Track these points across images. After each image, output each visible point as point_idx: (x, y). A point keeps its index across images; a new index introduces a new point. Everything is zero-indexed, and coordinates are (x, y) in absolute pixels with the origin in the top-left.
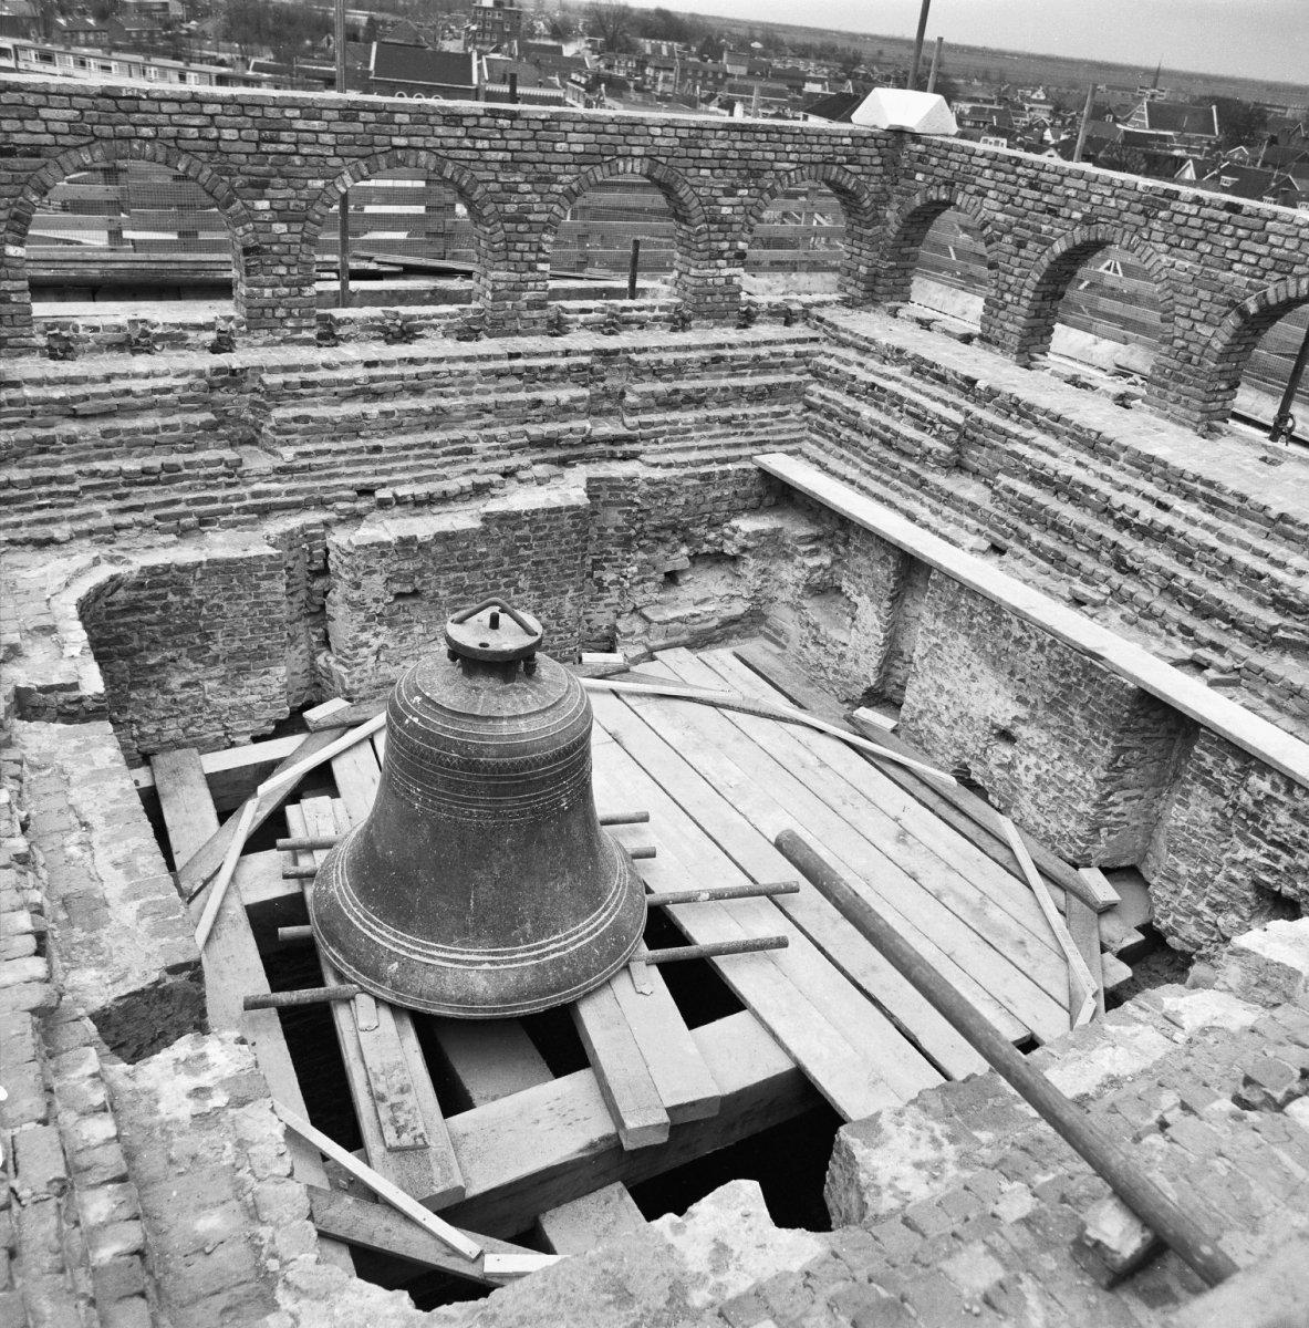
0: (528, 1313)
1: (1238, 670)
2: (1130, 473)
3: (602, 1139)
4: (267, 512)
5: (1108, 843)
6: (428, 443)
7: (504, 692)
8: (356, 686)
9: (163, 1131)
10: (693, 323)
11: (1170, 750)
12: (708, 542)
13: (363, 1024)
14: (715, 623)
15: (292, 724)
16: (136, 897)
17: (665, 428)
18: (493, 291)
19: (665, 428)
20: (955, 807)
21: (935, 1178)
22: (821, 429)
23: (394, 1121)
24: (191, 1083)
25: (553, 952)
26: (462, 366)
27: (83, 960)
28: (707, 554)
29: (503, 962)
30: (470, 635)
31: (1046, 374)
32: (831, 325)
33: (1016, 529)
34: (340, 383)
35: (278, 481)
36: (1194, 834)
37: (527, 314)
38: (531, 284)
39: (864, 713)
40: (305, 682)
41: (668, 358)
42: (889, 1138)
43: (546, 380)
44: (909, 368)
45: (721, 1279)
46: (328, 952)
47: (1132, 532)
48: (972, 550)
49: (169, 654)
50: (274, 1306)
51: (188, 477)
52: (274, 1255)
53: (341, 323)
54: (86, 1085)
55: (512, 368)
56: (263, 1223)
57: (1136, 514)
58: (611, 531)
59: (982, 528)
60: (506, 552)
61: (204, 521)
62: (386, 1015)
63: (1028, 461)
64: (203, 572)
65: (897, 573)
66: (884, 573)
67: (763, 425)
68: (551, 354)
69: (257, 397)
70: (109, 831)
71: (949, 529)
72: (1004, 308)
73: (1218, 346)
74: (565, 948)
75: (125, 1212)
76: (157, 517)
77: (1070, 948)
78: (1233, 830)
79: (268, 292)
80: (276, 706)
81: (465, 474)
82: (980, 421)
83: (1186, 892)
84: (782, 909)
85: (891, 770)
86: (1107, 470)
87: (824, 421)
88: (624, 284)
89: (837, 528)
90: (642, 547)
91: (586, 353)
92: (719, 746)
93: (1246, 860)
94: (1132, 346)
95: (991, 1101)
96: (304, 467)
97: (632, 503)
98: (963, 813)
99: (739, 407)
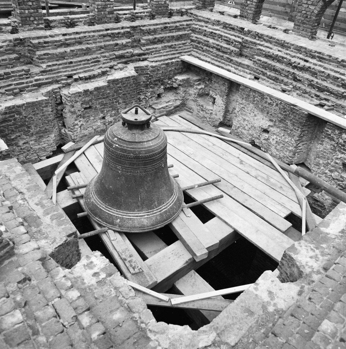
0: (226, 324)
1: (333, 106)
2: (295, 52)
3: (189, 260)
4: (40, 86)
5: (297, 157)
6: (86, 59)
7: (143, 134)
8: (75, 138)
9: (89, 289)
10: (156, 17)
11: (315, 130)
12: (168, 84)
13: (112, 239)
14: (172, 108)
15: (58, 151)
16: (48, 214)
17: (153, 50)
18: (97, 9)
19: (153, 50)
20: (252, 152)
21: (317, 260)
22: (197, 47)
23: (131, 266)
24: (92, 272)
25: (164, 209)
26: (92, 34)
27: (39, 237)
28: (168, 87)
29: (150, 214)
30: (130, 117)
31: (262, 25)
32: (195, 15)
33: (262, 72)
34: (56, 41)
35: (42, 75)
36: (325, 152)
37: (108, 16)
38: (109, 6)
39: (221, 129)
40: (58, 138)
41: (152, 28)
42: (300, 251)
43: (118, 37)
44: (222, 26)
45: (275, 302)
46: (95, 219)
47: (297, 69)
48: (250, 79)
49: (18, 134)
50: (148, 339)
51: (13, 76)
52: (142, 323)
53: (52, 21)
54: (63, 280)
55: (108, 34)
56: (134, 313)
57: (299, 64)
58: (142, 83)
59: (251, 72)
60: (115, 92)
61: (21, 90)
62: (118, 235)
63: (264, 51)
64: (25, 107)
65: (228, 88)
66: (224, 88)
67: (180, 47)
68: (118, 28)
69: (30, 48)
70: (30, 194)
71: (241, 73)
72: (247, 6)
73: (316, 12)
74: (167, 207)
75: (94, 321)
76: (6, 90)
77: (295, 187)
78: (337, 150)
79: (27, 11)
80: (52, 147)
81: (99, 68)
82: (247, 40)
83: (322, 168)
84: (216, 187)
85: (232, 144)
86: (288, 52)
87: (197, 45)
88: (132, 7)
89: (209, 75)
90: (151, 87)
91: (128, 28)
92: (184, 143)
93: (341, 157)
94: (273, 18)
95: (321, 235)
96: (50, 70)
97: (148, 74)
98: (255, 154)
99: (173, 42)
